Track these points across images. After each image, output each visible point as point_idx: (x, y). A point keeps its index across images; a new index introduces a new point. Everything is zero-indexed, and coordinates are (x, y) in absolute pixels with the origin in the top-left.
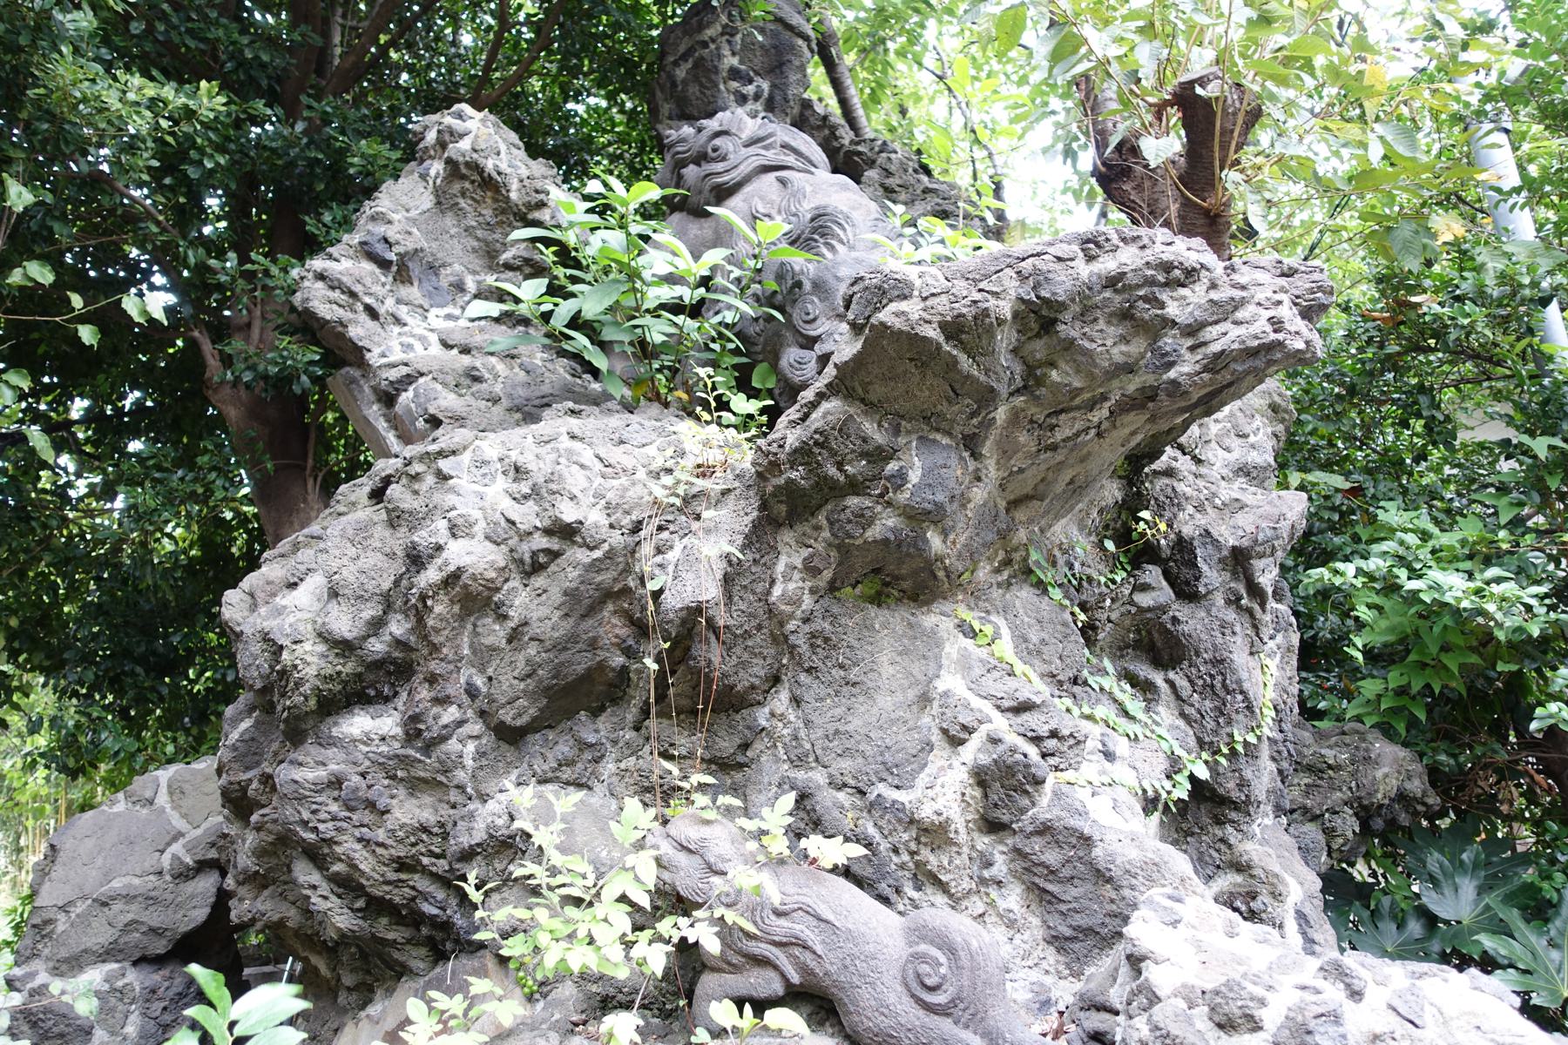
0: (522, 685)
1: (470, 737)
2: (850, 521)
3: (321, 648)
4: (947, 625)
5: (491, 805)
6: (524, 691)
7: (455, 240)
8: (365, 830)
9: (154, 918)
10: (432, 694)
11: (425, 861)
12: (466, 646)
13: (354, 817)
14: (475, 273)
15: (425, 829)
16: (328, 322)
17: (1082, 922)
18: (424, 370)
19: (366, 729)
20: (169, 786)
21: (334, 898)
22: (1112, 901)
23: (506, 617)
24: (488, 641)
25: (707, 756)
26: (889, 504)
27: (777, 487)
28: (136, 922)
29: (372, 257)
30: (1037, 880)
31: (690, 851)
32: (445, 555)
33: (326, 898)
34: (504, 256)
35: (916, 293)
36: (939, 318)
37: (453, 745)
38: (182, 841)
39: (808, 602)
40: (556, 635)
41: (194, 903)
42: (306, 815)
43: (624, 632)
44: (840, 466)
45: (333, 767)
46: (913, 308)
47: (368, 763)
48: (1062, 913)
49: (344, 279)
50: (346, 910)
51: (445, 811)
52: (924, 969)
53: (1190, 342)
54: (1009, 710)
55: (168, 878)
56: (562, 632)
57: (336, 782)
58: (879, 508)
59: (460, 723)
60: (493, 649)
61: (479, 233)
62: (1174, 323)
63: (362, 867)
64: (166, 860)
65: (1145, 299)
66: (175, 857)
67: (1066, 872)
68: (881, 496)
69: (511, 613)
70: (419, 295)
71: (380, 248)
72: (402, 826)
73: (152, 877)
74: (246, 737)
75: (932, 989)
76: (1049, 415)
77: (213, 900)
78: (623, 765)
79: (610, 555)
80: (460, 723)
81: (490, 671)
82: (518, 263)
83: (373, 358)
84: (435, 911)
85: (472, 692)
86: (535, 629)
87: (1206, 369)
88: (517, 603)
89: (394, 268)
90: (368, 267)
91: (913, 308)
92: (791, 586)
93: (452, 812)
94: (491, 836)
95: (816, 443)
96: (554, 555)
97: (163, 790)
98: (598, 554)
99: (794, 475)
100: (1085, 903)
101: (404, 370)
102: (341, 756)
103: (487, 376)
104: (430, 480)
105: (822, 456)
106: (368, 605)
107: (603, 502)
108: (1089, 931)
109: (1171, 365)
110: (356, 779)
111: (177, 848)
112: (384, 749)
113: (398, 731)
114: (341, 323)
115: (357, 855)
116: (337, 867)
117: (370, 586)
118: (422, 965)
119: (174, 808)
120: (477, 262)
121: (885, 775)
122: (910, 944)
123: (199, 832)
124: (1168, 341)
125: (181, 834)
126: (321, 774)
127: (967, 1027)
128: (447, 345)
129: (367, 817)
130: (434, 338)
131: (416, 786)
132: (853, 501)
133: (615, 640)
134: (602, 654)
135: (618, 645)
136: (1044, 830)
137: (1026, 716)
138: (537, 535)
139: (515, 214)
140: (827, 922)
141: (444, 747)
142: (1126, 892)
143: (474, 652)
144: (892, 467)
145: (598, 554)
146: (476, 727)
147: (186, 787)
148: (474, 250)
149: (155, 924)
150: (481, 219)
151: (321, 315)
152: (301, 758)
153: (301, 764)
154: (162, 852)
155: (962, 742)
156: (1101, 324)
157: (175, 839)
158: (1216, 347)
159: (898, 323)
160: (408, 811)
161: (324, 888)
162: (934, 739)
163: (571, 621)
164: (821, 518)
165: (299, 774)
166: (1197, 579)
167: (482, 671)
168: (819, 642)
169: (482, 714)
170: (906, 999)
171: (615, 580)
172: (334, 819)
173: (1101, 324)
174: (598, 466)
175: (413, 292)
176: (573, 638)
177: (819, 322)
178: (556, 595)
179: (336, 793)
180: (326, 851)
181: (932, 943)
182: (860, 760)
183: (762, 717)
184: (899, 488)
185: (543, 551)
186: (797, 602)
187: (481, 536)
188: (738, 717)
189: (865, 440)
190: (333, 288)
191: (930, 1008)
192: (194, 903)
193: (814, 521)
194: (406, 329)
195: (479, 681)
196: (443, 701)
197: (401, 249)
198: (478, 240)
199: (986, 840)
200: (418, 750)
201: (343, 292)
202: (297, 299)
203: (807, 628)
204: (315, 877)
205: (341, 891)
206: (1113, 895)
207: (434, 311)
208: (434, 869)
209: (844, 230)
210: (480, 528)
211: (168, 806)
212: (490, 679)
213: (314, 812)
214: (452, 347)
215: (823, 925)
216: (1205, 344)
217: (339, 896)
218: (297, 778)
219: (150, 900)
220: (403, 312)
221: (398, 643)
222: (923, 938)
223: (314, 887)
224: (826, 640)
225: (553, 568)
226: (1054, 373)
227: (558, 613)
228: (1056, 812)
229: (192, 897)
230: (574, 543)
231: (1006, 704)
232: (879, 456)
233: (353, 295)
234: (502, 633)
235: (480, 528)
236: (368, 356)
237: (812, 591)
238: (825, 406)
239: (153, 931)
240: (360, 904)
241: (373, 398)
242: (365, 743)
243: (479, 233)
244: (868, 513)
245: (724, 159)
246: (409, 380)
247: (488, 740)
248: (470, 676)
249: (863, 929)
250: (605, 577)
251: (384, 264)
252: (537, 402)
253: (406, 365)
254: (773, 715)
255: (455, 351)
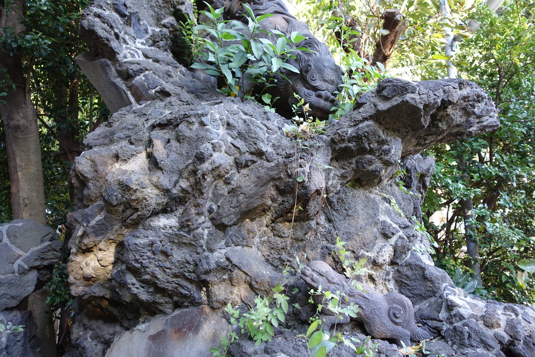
0: (234, 210)
1: (206, 228)
2: (366, 163)
3: (156, 191)
4: (378, 198)
5: (216, 254)
6: (234, 212)
7: (146, 10)
8: (160, 263)
9: (13, 292)
10: (197, 211)
11: (186, 274)
12: (211, 193)
13: (156, 257)
14: (151, 26)
15: (188, 262)
16: (101, 38)
17: (417, 293)
18: (148, 68)
19: (166, 223)
20: (8, 234)
21: (141, 288)
22: (430, 287)
23: (229, 184)
24: (221, 192)
25: (293, 237)
26: (381, 159)
27: (341, 148)
28: (5, 294)
29: (117, 11)
30: (402, 280)
31: (323, 276)
32: (212, 158)
33: (137, 288)
34: (164, 21)
35: (417, 92)
36: (424, 103)
37: (200, 230)
38: (21, 259)
39: (339, 187)
40: (251, 192)
41: (28, 284)
42: (138, 257)
43: (274, 193)
44: (369, 144)
45: (151, 238)
46: (416, 96)
47: (164, 237)
48: (409, 290)
49: (110, 20)
50: (146, 293)
51: (195, 255)
52: (397, 312)
53: (478, 121)
54: (403, 228)
55: (17, 274)
56: (253, 192)
57: (152, 244)
58: (377, 160)
59: (204, 222)
60: (223, 195)
61: (156, 9)
62: (475, 114)
63: (159, 277)
64: (15, 267)
65: (471, 105)
66: (19, 265)
67: (413, 278)
68: (379, 156)
69: (233, 183)
70: (133, 32)
71: (122, 8)
72: (178, 261)
73: (10, 275)
74: (100, 223)
75: (397, 318)
76: (426, 135)
77: (36, 282)
78: (262, 239)
79: (277, 165)
80: (204, 222)
81: (219, 204)
82: (169, 25)
83: (120, 57)
84: (187, 292)
85: (210, 211)
86: (245, 190)
87: (480, 130)
88: (235, 179)
89: (126, 18)
90: (116, 15)
91: (416, 96)
92: (335, 182)
93: (198, 256)
94: (218, 266)
95: (365, 136)
96: (254, 162)
97: (5, 236)
98: (272, 164)
99: (350, 145)
100: (419, 287)
101: (139, 67)
102: (154, 234)
103: (173, 75)
104: (196, 125)
105: (364, 140)
106: (174, 175)
107: (271, 144)
108: (420, 295)
109: (472, 126)
110: (159, 243)
111: (19, 261)
112: (171, 231)
113: (177, 224)
114: (108, 40)
115: (157, 272)
116: (147, 277)
117: (175, 167)
118: (170, 311)
119: (12, 244)
120: (152, 21)
121: (363, 247)
122: (389, 304)
123: (28, 254)
124: (471, 119)
125: (21, 256)
126: (146, 241)
127: (405, 328)
128: (146, 56)
129: (162, 258)
130: (140, 53)
131: (181, 245)
132: (369, 156)
133: (270, 195)
134: (265, 200)
135: (271, 197)
136: (409, 265)
137: (407, 230)
138: (247, 154)
139: (171, 5)
140: (367, 298)
141: (196, 231)
142: (437, 285)
143: (214, 196)
144: (385, 147)
145: (272, 164)
146: (209, 224)
147: (17, 234)
148: (152, 16)
149: (13, 295)
150: (157, 3)
151: (99, 34)
152: (138, 235)
153: (138, 237)
154: (13, 263)
155: (390, 238)
156: (457, 111)
157: (18, 258)
158: (485, 123)
159: (412, 102)
160: (179, 255)
161: (138, 284)
162: (377, 236)
163: (257, 187)
164: (354, 160)
165: (138, 241)
166: (411, 182)
167: (216, 203)
168: (340, 201)
169: (212, 219)
170: (390, 321)
171: (277, 174)
172: (149, 258)
173: (457, 111)
174: (265, 129)
175: (130, 30)
176: (256, 194)
177: (316, 81)
178: (253, 178)
179: (150, 248)
180: (143, 270)
181: (397, 304)
182: (354, 242)
183: (313, 223)
184: (387, 154)
185: (250, 160)
186: (335, 187)
187: (223, 151)
188: (304, 224)
189: (379, 137)
190: (104, 23)
191: (396, 323)
192: (28, 284)
193: (350, 161)
194: (128, 46)
195: (214, 207)
196: (199, 214)
197: (132, 11)
198: (155, 12)
199: (390, 268)
200: (185, 232)
201: (108, 25)
202: (85, 23)
203: (337, 196)
204: (134, 280)
205: (144, 285)
206: (431, 285)
207: (138, 40)
208: (190, 277)
209: (318, 46)
210: (224, 148)
211: (8, 243)
212: (219, 206)
213: (141, 256)
214: (149, 58)
215: (365, 299)
216: (482, 122)
217: (143, 287)
218: (136, 242)
219: (10, 284)
220: (127, 37)
221: (183, 190)
222: (394, 302)
223: (134, 284)
224: (343, 200)
225: (252, 167)
226: (440, 124)
227: (253, 185)
228: (413, 260)
229: (28, 282)
230: (262, 159)
231: (403, 226)
232: (383, 142)
233: (112, 27)
234: (226, 190)
235: (224, 148)
236: (118, 56)
237: (341, 184)
238: (366, 123)
239: (13, 297)
240: (151, 290)
241: (116, 74)
242: (163, 229)
243: (156, 9)
244: (373, 161)
245: (262, 4)
246: (141, 71)
247: (213, 229)
248: (211, 205)
249: (377, 300)
250: (273, 173)
251: (123, 15)
252: (201, 91)
253: (139, 64)
254: (318, 224)
255: (151, 60)
